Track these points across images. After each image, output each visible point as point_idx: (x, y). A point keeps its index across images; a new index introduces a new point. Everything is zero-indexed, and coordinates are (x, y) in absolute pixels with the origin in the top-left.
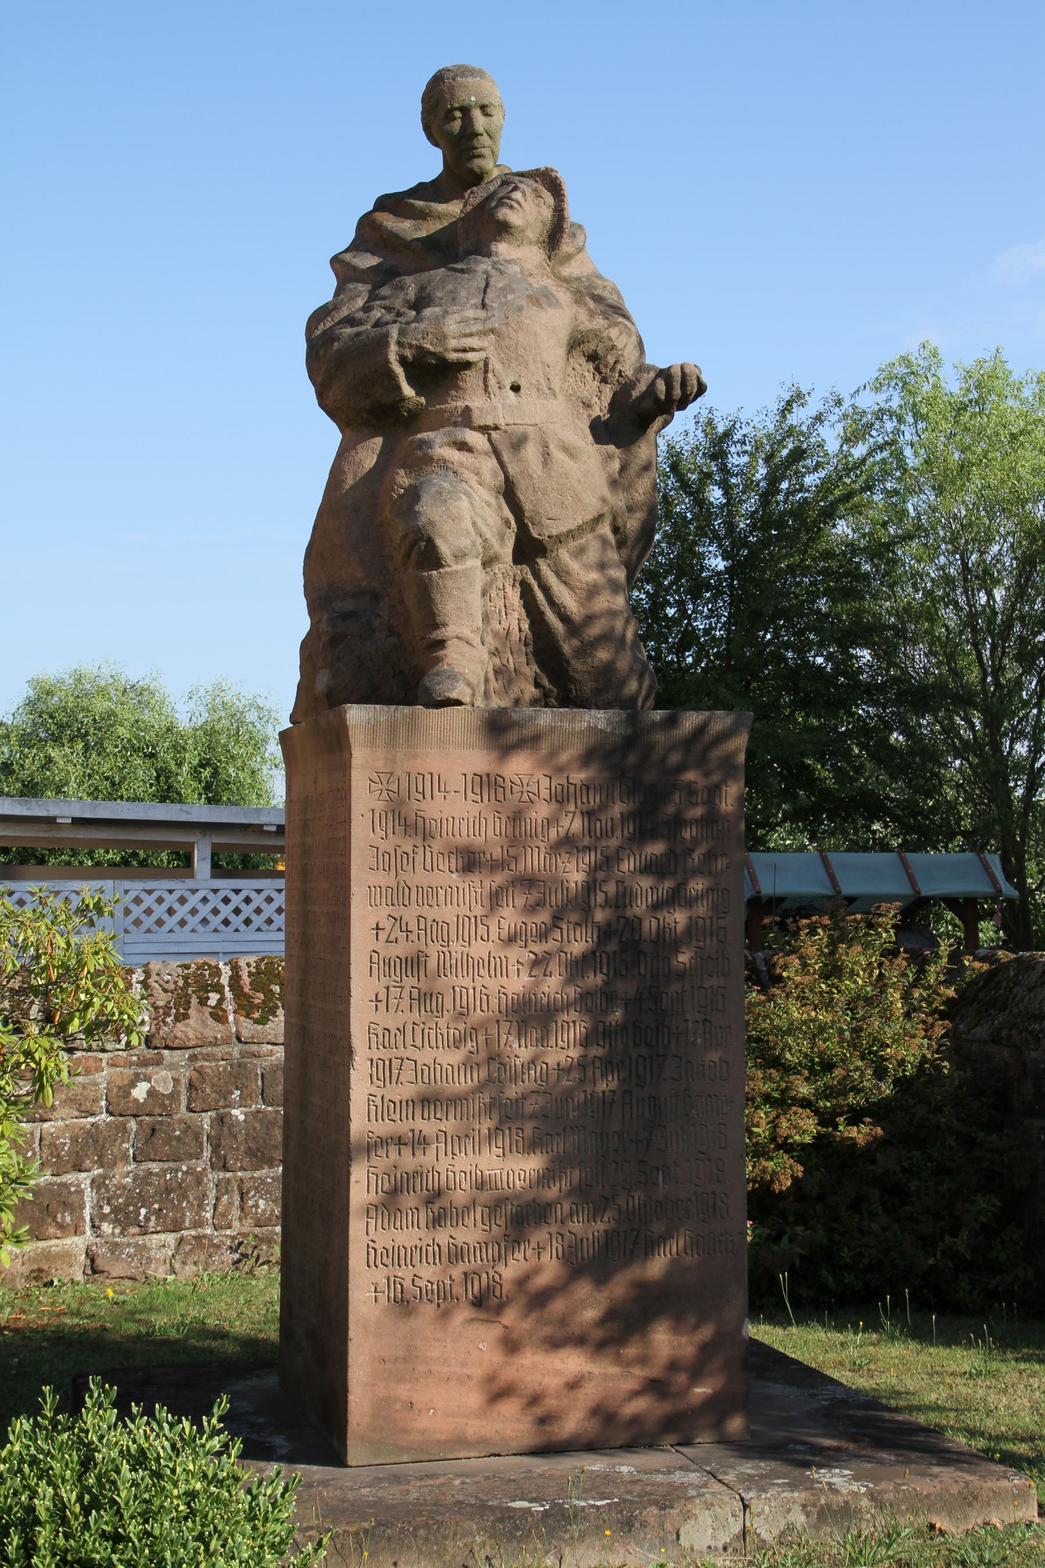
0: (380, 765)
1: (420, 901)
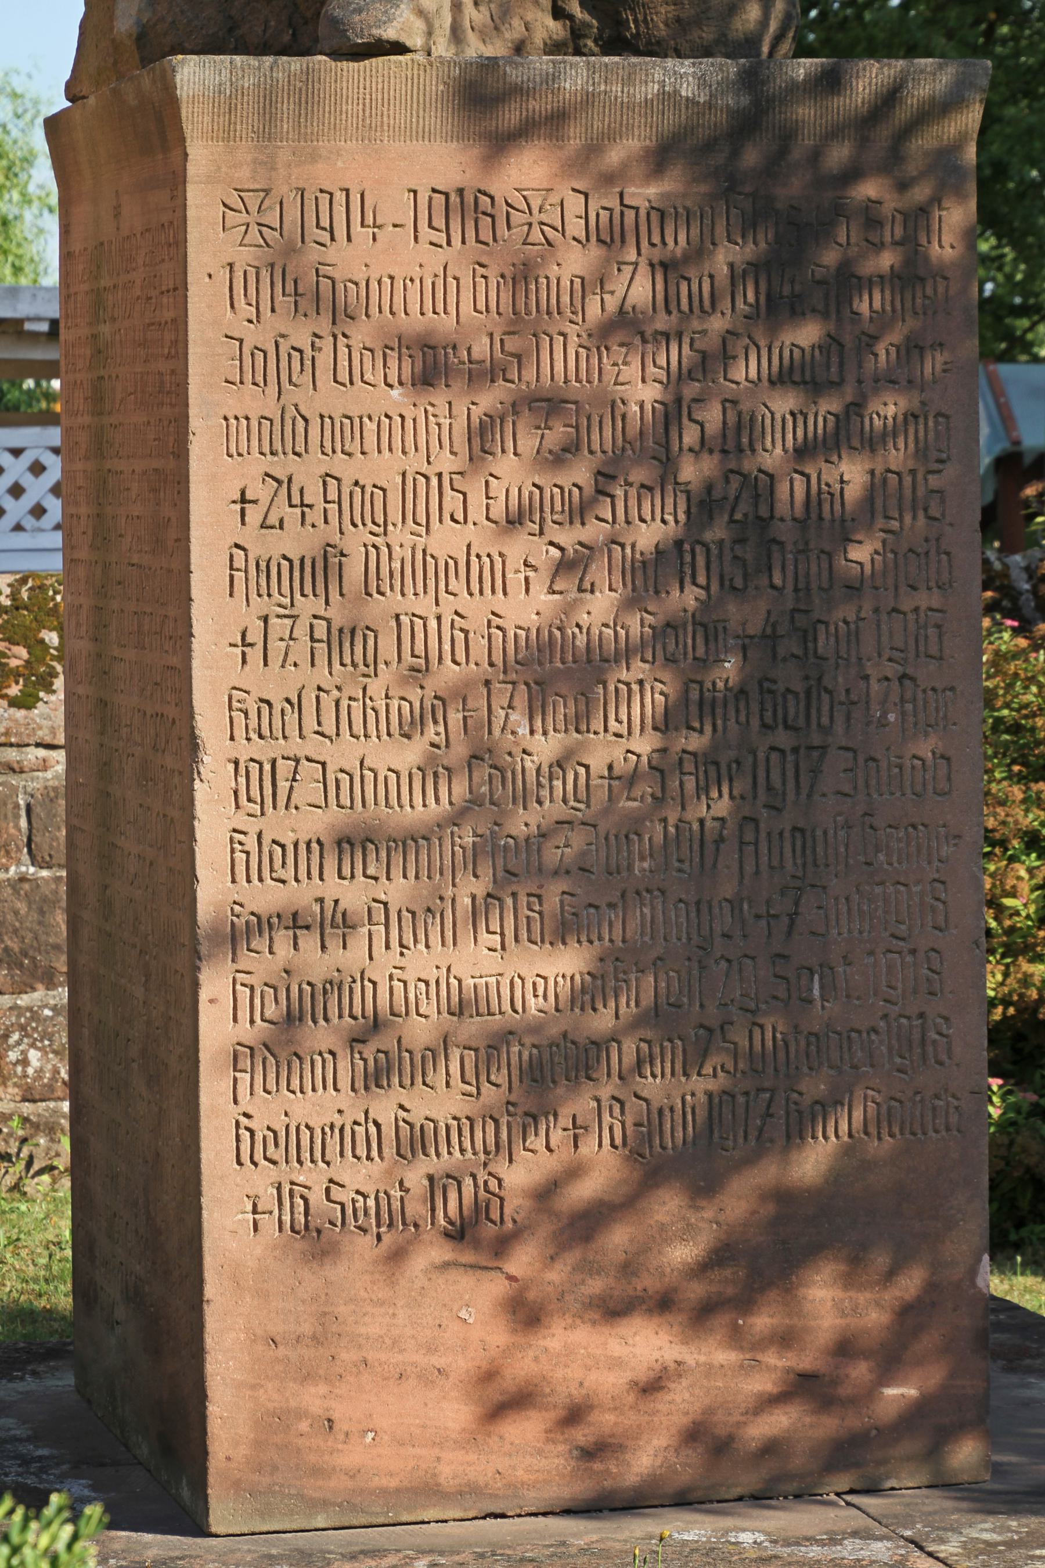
0: (243, 176)
1: (328, 444)
